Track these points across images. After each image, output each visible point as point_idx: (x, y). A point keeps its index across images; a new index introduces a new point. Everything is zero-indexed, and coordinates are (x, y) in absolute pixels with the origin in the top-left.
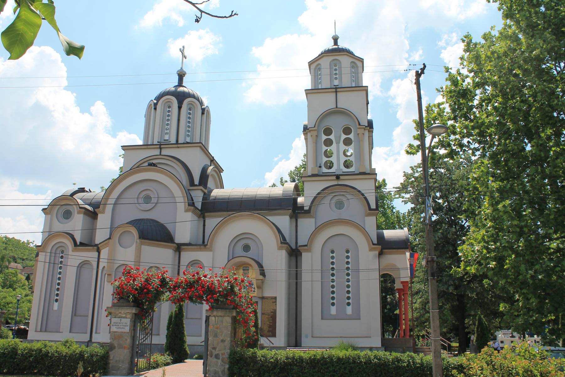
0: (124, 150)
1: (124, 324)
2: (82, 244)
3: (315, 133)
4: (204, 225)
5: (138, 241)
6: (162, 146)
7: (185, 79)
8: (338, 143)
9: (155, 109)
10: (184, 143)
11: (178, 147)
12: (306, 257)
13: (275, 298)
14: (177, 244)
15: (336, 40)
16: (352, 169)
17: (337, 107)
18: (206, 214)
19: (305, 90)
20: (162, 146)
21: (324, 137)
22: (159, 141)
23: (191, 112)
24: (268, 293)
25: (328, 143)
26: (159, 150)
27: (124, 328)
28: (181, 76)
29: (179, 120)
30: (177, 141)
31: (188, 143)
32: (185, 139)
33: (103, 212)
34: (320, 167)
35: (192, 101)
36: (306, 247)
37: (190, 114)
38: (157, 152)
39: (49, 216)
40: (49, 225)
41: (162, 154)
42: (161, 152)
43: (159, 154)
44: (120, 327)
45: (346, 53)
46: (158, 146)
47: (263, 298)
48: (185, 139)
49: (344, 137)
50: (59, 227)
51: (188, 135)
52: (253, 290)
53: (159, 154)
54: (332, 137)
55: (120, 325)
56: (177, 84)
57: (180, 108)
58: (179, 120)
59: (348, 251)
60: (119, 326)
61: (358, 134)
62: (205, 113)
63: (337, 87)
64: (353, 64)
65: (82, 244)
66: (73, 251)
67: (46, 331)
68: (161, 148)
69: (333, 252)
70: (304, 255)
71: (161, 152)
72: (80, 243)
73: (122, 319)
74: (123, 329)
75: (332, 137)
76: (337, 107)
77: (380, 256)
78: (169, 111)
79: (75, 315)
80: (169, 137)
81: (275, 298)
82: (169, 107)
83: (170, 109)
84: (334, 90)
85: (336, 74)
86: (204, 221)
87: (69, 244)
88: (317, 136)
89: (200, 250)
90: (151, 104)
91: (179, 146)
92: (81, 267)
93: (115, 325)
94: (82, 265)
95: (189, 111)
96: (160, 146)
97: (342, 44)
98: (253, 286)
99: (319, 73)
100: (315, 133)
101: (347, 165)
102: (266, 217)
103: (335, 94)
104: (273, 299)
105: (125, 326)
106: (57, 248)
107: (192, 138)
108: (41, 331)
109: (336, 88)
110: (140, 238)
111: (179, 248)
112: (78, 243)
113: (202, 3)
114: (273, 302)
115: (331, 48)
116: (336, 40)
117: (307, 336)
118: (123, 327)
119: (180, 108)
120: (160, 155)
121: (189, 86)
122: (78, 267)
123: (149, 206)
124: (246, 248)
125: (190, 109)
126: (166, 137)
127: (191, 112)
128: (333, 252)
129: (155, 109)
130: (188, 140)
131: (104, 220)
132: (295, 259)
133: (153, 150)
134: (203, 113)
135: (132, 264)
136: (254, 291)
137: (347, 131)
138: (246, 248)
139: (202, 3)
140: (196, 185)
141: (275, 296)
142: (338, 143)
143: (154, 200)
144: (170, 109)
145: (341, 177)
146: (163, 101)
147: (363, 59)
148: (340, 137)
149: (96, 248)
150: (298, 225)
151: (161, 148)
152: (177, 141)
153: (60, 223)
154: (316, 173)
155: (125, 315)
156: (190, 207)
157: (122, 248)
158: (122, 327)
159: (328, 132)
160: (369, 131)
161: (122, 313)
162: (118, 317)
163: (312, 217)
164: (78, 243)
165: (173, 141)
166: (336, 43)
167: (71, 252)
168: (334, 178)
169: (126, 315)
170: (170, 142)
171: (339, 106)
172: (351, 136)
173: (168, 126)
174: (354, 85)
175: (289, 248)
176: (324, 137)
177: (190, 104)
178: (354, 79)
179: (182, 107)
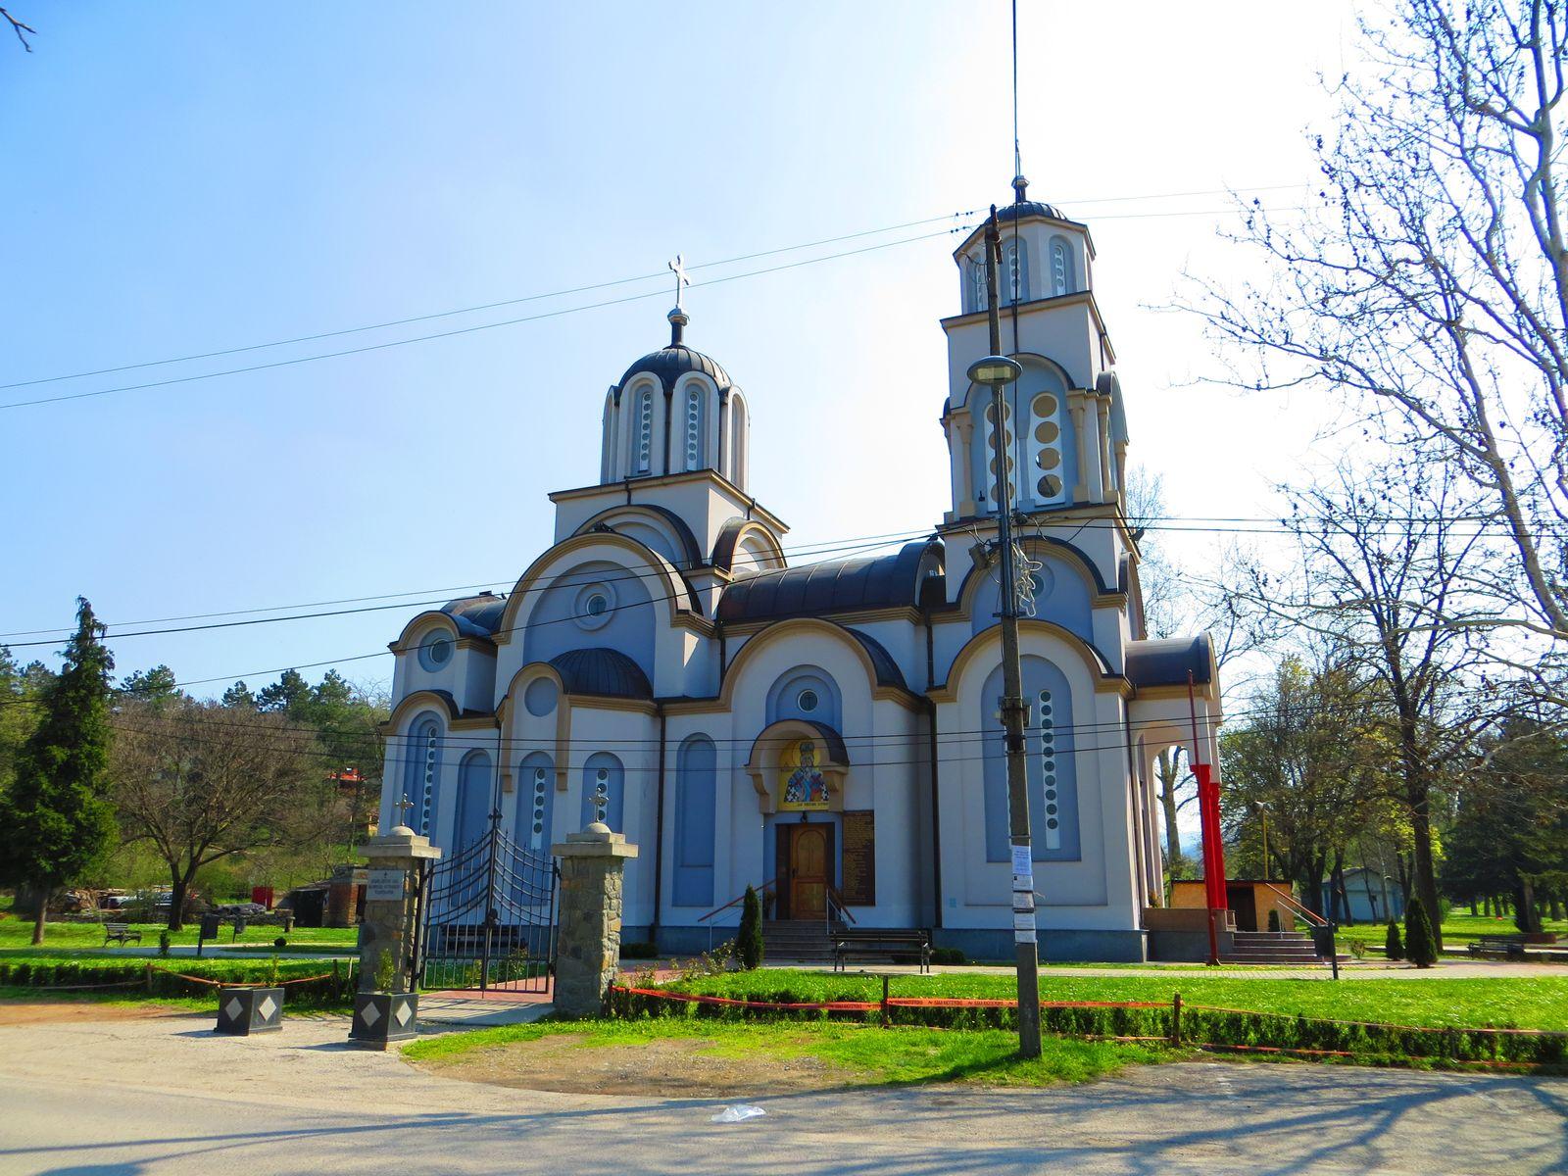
2: (469, 713)
3: (966, 421)
7: (685, 329)
11: (665, 485)
12: (946, 716)
13: (1079, 859)
14: (657, 701)
16: (1059, 498)
18: (726, 628)
20: (630, 487)
28: (677, 322)
30: (666, 470)
31: (690, 473)
32: (685, 464)
33: (507, 641)
34: (982, 499)
36: (944, 691)
39: (403, 658)
40: (402, 675)
41: (633, 502)
43: (626, 503)
45: (1039, 218)
46: (623, 487)
47: (845, 814)
48: (685, 464)
50: (424, 680)
56: (670, 344)
57: (668, 396)
66: (450, 729)
68: (629, 491)
70: (942, 710)
72: (465, 710)
77: (1130, 704)
81: (1079, 859)
87: (440, 711)
88: (971, 426)
92: (468, 765)
94: (471, 760)
96: (628, 485)
97: (1032, 196)
100: (966, 421)
101: (1046, 487)
105: (394, 887)
106: (424, 724)
107: (701, 461)
111: (661, 709)
112: (461, 712)
113: (1486, 334)
114: (866, 823)
116: (1020, 186)
117: (953, 903)
119: (668, 396)
120: (629, 504)
122: (460, 765)
123: (604, 618)
124: (809, 700)
125: (694, 397)
126: (644, 465)
130: (692, 466)
131: (510, 657)
132: (929, 718)
133: (606, 497)
135: (549, 747)
138: (809, 700)
139: (1498, 342)
140: (707, 566)
143: (611, 606)
146: (633, 385)
147: (1085, 226)
149: (492, 719)
151: (629, 491)
152: (666, 470)
153: (425, 669)
154: (970, 513)
157: (530, 715)
160: (1098, 401)
163: (966, 619)
164: (461, 712)
165: (657, 470)
167: (447, 733)
171: (1022, 349)
174: (1061, 291)
175: (906, 697)
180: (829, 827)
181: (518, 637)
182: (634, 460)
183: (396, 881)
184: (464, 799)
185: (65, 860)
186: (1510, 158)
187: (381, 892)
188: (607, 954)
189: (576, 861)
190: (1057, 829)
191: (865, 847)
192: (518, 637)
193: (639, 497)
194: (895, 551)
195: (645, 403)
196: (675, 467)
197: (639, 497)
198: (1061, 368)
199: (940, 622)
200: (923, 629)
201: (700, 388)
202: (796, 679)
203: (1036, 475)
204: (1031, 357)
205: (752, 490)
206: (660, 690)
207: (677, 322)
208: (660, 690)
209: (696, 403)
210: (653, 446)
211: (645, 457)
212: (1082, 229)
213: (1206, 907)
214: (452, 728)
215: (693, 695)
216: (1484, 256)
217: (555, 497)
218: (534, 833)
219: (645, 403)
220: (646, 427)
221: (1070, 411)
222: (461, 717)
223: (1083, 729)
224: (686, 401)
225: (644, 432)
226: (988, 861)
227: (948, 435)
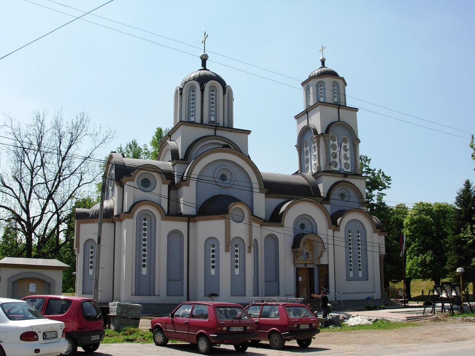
0: (296, 119)
24: (323, 261)
29: (202, 101)
35: (213, 83)
43: (214, 135)
52: (310, 259)
53: (214, 135)
57: (202, 90)
58: (202, 101)
62: (227, 93)
63: (218, 125)
67: (139, 295)
79: (169, 280)
80: (216, 118)
82: (193, 91)
83: (194, 93)
84: (215, 128)
90: (177, 90)
98: (310, 256)
108: (135, 295)
109: (216, 126)
119: (202, 90)
121: (213, 67)
125: (213, 91)
126: (213, 119)
129: (181, 94)
134: (224, 93)
136: (311, 260)
144: (194, 93)
147: (343, 78)
150: (189, 261)
165: (198, 121)
170: (219, 124)
173: (322, 90)
180: (311, 270)
184: (276, 262)
185: (463, 240)
186: (35, 218)
194: (30, 210)
195: (192, 93)
196: (206, 121)
201: (215, 87)
204: (342, 123)
207: (204, 60)
209: (214, 93)
210: (196, 115)
211: (192, 116)
213: (321, 264)
214: (163, 219)
216: (25, 210)
219: (192, 93)
220: (193, 99)
223: (341, 240)
224: (210, 92)
225: (192, 101)
226: (368, 280)
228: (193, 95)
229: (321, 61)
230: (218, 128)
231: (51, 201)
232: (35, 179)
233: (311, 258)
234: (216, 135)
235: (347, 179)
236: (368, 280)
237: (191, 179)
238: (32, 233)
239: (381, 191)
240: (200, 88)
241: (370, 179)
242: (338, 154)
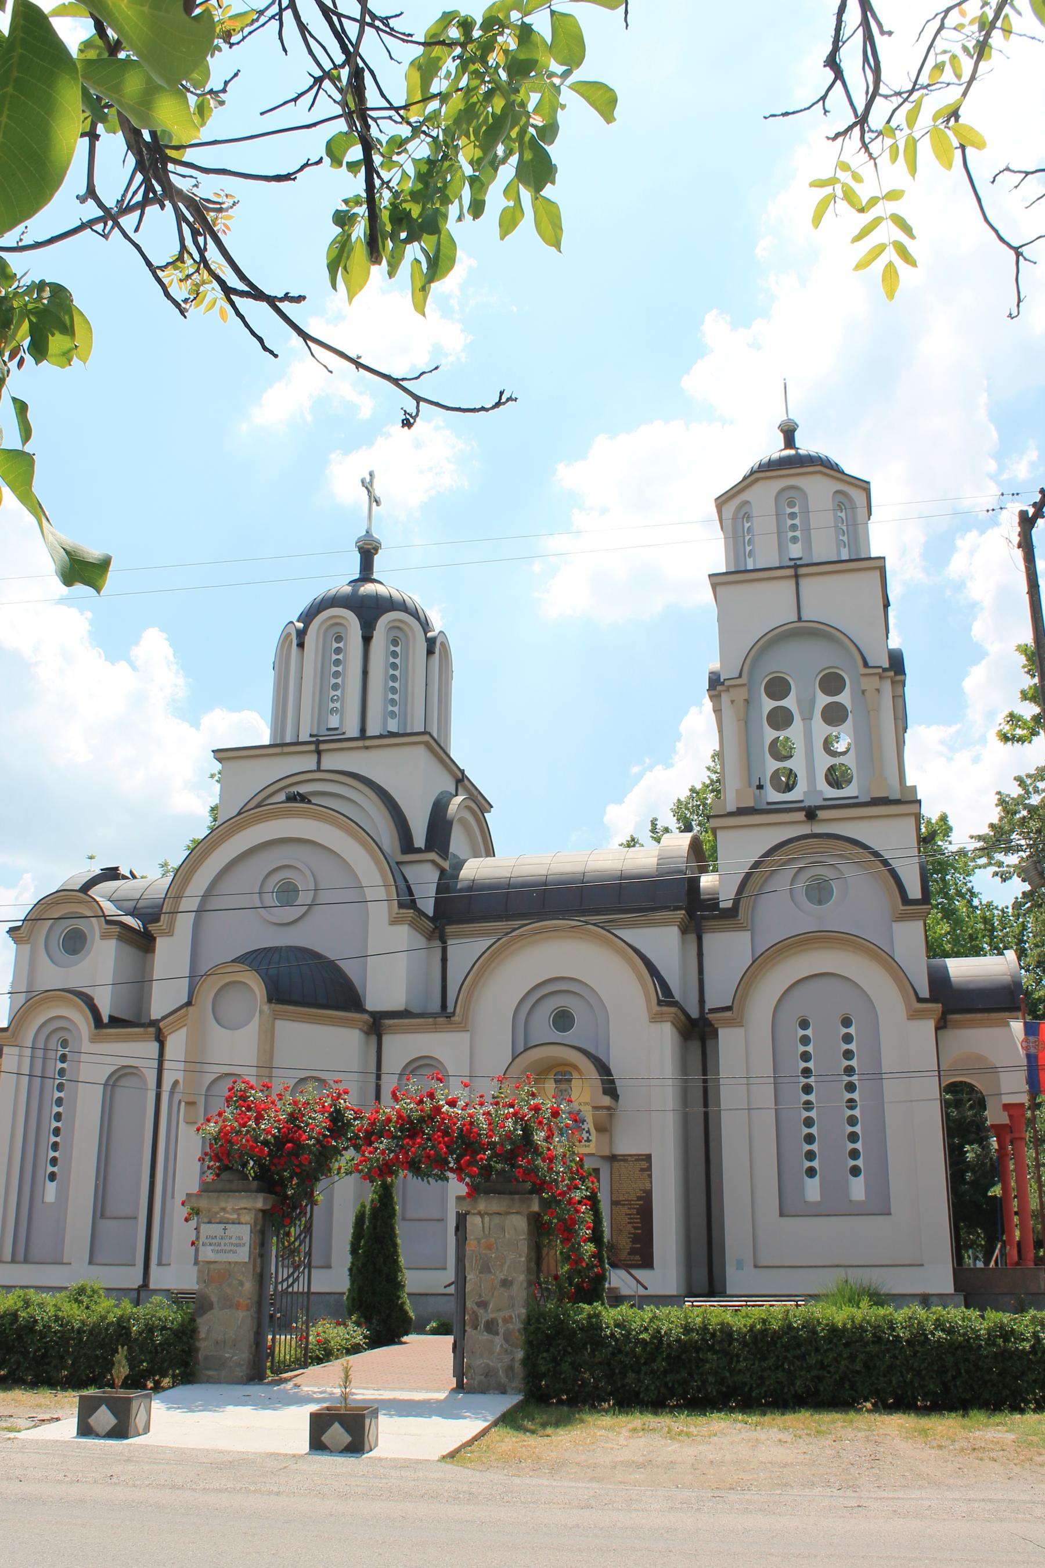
1: (234, 1241)
2: (115, 1022)
3: (741, 694)
4: (444, 960)
5: (266, 1008)
6: (322, 747)
8: (807, 718)
9: (301, 645)
10: (381, 737)
11: (367, 748)
12: (728, 1040)
14: (374, 1014)
15: (789, 434)
16: (850, 791)
17: (800, 619)
18: (449, 929)
19: (710, 576)
20: (322, 747)
21: (768, 704)
22: (315, 732)
23: (398, 649)
25: (781, 719)
26: (314, 758)
27: (235, 1252)
28: (368, 553)
29: (365, 673)
30: (363, 730)
31: (392, 735)
32: (385, 724)
33: (169, 932)
34: (760, 787)
36: (728, 1014)
37: (394, 654)
38: (309, 762)
41: (322, 768)
42: (319, 762)
44: (223, 1247)
48: (385, 724)
49: (823, 700)
51: (393, 714)
52: (585, 1135)
54: (789, 702)
55: (223, 1242)
57: (367, 639)
58: (365, 673)
59: (847, 1022)
60: (219, 1244)
61: (863, 692)
62: (437, 650)
63: (799, 562)
64: (842, 499)
65: (115, 1022)
67: (26, 1261)
68: (319, 752)
69: (804, 1024)
71: (319, 762)
73: (228, 1226)
74: (231, 1255)
75: (789, 702)
76: (800, 619)
78: (338, 651)
79: (103, 1216)
82: (339, 639)
83: (341, 645)
84: (791, 572)
85: (794, 527)
86: (444, 951)
87: (82, 1021)
89: (436, 1028)
90: (289, 634)
91: (368, 743)
92: (114, 1086)
93: (210, 1244)
95: (393, 648)
96: (318, 745)
97: (807, 444)
98: (585, 1126)
99: (747, 525)
100: (741, 694)
101: (836, 778)
102: (613, 931)
103: (792, 583)
104: (643, 1160)
105: (238, 1245)
107: (403, 722)
110: (270, 1000)
112: (106, 1020)
114: (642, 1170)
115: (776, 456)
116: (789, 434)
117: (740, 1265)
118: (232, 1248)
119: (367, 639)
120: (319, 769)
122: (105, 1085)
124: (563, 1020)
125: (395, 642)
126: (334, 722)
127: (398, 649)
128: (804, 1024)
130: (393, 726)
134: (430, 652)
136: (588, 1140)
137: (832, 683)
140: (419, 851)
141: (648, 1152)
142: (807, 718)
144: (341, 645)
145: (821, 814)
147: (868, 483)
148: (813, 702)
149: (152, 1030)
151: (319, 752)
152: (363, 730)
153: (53, 962)
154: (749, 803)
155: (235, 1216)
156: (405, 911)
158: (228, 1248)
159: (778, 688)
160: (893, 683)
161: (229, 1208)
162: (218, 1220)
164: (106, 1020)
166: (789, 441)
167: (86, 1046)
168: (801, 816)
169: (239, 1215)
170: (344, 733)
172: (844, 698)
174: (845, 556)
176: (768, 704)
177: (395, 627)
178: (845, 538)
179: (372, 637)
181: (184, 923)
182: (322, 711)
183: (239, 1238)
187: (221, 1251)
188: (1000, 1314)
189: (487, 1219)
190: (55, 1182)
191: (639, 1198)
192: (184, 923)
193: (330, 762)
195: (335, 645)
196: (370, 732)
197: (330, 762)
198: (856, 646)
199: (714, 930)
200: (692, 937)
202: (588, 1002)
203: (823, 762)
205: (458, 753)
206: (373, 1003)
207: (368, 553)
208: (373, 1003)
212: (864, 486)
214: (93, 1040)
215: (415, 1010)
217: (213, 751)
218: (808, 1180)
219: (335, 645)
221: (863, 692)
222: (106, 1026)
227: (717, 711)
228: (338, 651)
229: (782, 431)
230: (802, 571)
231: (821, 102)
232: (170, 270)
233: (587, 1132)
234: (322, 768)
235: (818, 829)
236: (329, 1267)
237: (884, 1076)
238: (526, 162)
239: (879, 35)
240: (360, 632)
241: (985, 1329)
242: (793, 1497)
